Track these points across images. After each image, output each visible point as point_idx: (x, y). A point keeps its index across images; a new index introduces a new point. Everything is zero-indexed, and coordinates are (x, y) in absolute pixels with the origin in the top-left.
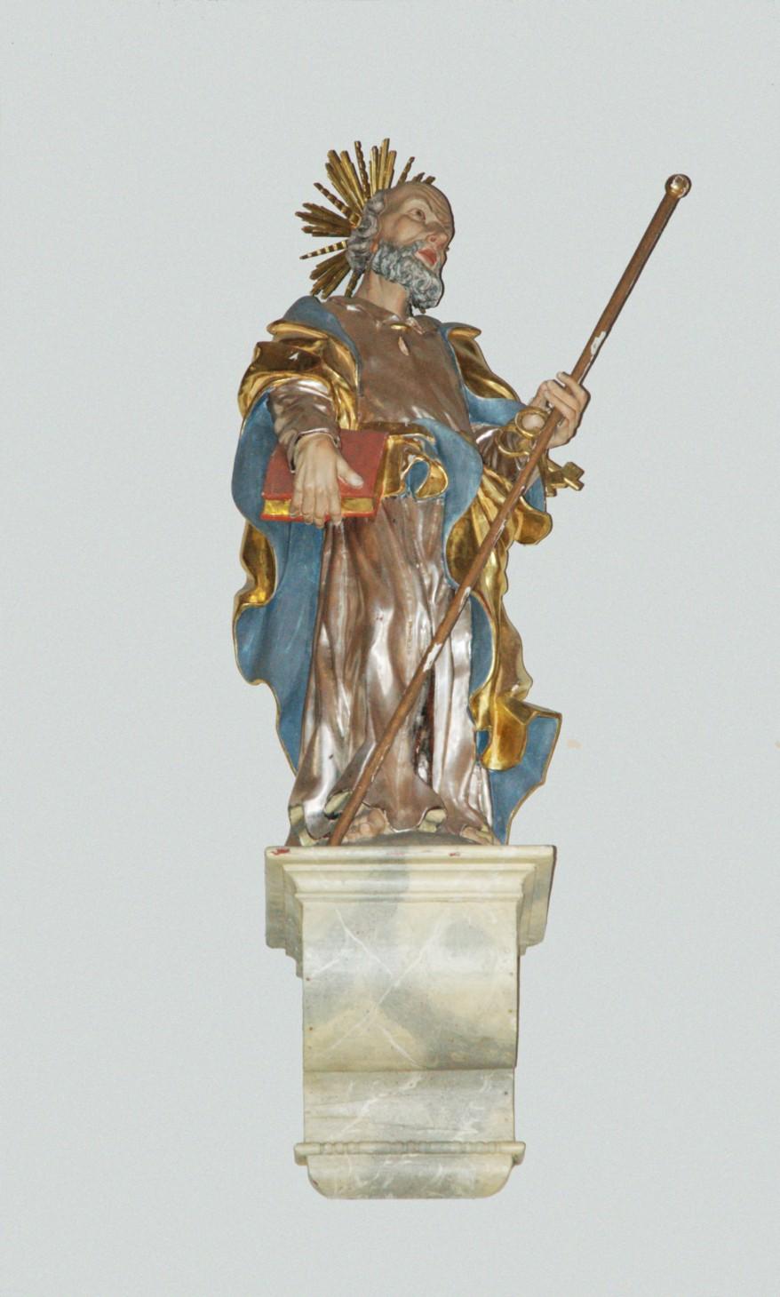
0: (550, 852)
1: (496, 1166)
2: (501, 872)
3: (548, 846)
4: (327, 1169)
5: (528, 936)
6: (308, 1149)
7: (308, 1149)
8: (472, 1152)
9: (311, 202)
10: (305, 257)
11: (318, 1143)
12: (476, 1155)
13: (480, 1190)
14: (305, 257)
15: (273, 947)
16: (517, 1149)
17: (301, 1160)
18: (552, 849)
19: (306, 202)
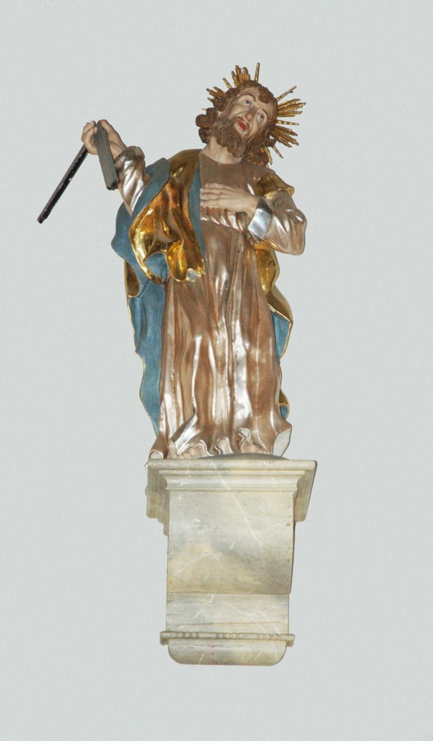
0: (313, 465)
1: (272, 648)
2: (274, 476)
3: (312, 461)
4: (182, 646)
5: (299, 515)
6: (168, 635)
7: (168, 635)
8: (230, 639)
9: (219, 87)
10: (280, 156)
11: (255, 634)
12: (172, 639)
13: (267, 661)
14: (280, 156)
15: (150, 517)
16: (290, 638)
17: (164, 641)
18: (314, 464)
19: (215, 86)
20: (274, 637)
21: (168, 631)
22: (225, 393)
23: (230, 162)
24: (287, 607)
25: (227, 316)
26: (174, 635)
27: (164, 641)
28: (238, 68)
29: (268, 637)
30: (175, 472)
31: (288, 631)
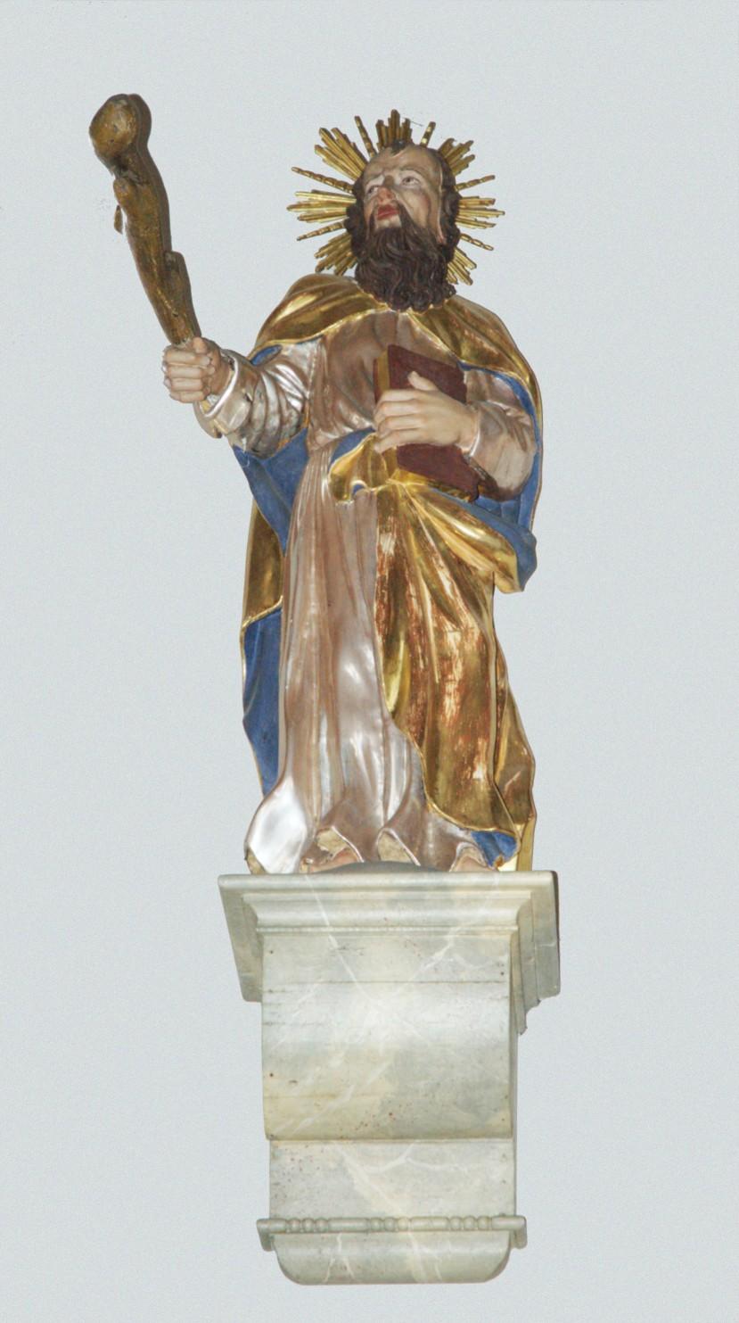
0: (548, 879)
3: (546, 871)
16: (514, 1223)
20: (482, 1224)
21: (274, 1219)
22: (335, 467)
23: (308, 614)
24: (512, 1162)
25: (334, 550)
26: (280, 1226)
27: (267, 1241)
28: (395, 115)
29: (469, 1223)
30: (273, 895)
31: (515, 1211)
